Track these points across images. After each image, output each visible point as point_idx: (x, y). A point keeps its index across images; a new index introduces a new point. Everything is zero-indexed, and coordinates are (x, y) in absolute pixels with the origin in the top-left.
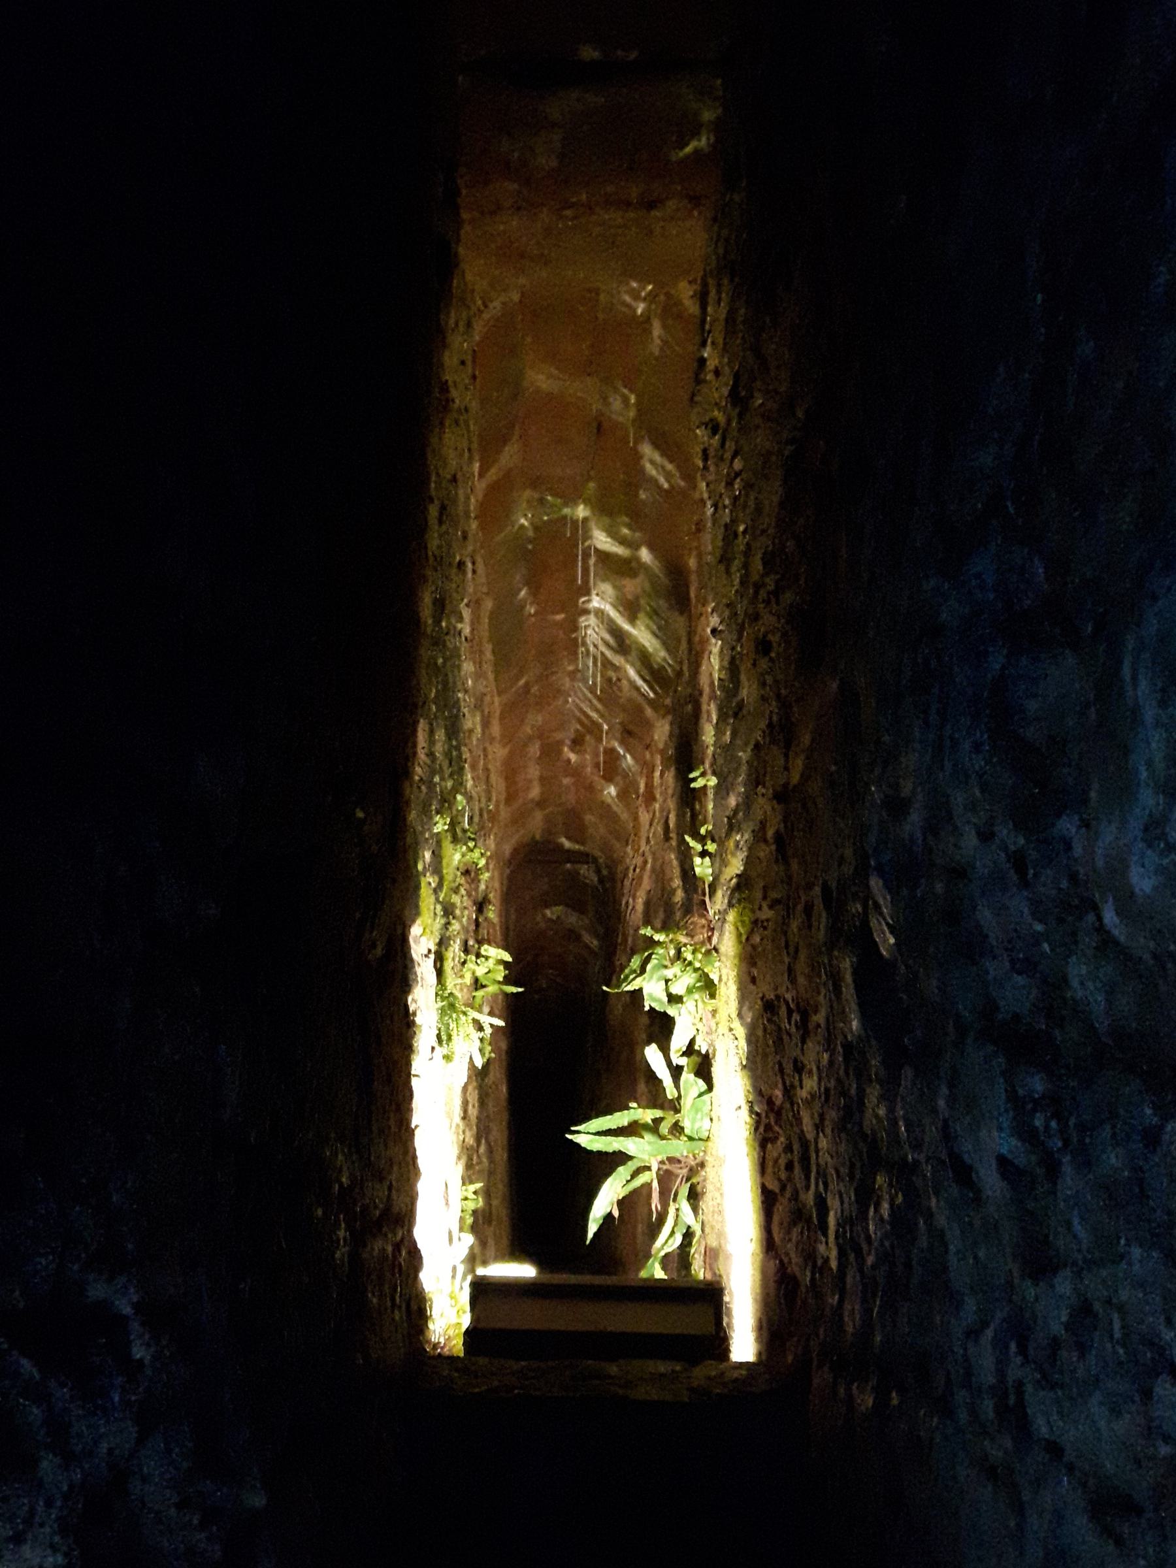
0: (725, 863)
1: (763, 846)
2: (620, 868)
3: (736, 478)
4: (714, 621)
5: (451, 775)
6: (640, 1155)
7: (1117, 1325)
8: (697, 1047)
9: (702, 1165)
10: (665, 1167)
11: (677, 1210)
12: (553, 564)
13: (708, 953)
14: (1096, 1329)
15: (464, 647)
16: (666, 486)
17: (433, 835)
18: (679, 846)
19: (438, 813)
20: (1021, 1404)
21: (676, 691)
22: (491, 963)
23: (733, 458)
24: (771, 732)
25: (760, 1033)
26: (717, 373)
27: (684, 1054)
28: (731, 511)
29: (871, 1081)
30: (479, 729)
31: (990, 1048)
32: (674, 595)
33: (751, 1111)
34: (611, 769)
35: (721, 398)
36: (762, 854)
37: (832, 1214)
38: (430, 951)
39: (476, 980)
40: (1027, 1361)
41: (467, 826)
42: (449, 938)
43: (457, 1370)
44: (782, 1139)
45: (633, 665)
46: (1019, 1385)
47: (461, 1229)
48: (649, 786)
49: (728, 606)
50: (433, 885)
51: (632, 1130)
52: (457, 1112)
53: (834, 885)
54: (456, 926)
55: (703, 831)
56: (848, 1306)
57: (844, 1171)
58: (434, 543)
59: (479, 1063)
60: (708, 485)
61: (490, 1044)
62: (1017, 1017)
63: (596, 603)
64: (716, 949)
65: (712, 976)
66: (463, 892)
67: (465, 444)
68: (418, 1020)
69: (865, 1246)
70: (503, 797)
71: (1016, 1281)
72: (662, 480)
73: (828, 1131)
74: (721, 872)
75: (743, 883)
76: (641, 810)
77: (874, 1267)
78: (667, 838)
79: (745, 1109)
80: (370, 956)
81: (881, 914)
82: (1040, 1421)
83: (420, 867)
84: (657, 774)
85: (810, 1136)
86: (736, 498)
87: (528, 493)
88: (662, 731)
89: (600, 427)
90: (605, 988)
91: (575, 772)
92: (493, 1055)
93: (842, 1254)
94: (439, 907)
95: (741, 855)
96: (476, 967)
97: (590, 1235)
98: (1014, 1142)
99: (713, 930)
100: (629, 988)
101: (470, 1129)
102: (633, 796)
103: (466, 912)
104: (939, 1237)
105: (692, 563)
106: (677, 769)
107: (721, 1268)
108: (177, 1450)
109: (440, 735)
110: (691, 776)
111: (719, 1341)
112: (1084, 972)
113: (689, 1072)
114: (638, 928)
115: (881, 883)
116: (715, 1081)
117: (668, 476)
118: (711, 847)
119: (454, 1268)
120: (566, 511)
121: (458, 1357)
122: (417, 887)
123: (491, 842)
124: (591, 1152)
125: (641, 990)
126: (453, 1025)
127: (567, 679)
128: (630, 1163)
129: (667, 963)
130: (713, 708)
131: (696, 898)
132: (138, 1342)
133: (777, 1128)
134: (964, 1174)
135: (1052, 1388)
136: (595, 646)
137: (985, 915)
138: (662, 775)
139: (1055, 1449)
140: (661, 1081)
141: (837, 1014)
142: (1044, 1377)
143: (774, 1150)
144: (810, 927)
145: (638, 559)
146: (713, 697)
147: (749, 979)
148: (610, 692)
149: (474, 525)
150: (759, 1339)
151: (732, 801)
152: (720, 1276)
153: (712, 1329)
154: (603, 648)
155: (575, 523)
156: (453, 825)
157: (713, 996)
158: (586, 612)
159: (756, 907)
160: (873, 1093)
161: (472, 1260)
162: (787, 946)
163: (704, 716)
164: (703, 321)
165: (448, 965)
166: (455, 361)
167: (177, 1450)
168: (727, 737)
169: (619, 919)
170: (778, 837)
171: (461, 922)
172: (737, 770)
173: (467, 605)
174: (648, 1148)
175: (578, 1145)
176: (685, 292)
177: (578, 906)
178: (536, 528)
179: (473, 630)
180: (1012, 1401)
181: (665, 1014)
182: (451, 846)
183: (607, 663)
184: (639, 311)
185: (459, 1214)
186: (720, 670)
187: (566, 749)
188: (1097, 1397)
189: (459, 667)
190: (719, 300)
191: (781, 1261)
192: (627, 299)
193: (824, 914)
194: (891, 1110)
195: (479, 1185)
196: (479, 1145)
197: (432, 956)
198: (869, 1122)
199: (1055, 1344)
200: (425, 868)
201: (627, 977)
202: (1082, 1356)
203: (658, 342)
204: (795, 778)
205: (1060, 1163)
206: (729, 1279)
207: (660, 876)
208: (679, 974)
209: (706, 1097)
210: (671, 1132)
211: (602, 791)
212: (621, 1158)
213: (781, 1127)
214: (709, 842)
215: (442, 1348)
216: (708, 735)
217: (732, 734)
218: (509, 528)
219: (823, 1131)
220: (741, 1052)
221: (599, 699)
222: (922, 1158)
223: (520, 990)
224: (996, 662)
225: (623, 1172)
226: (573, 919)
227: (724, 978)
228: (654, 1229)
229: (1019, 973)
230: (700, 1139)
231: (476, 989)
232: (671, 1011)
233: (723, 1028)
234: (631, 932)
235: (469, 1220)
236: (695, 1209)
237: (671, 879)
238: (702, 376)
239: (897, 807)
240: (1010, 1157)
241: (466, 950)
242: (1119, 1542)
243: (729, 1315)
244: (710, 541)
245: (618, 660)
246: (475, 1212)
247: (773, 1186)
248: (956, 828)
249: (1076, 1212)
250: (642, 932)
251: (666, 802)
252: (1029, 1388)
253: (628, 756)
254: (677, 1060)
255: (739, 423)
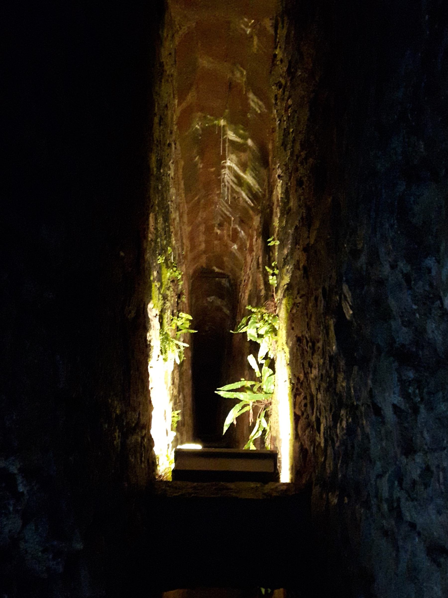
0: (282, 279)
1: (298, 271)
2: (239, 280)
3: (289, 108)
4: (279, 172)
5: (165, 239)
6: (245, 400)
7: (441, 478)
8: (269, 356)
9: (270, 403)
10: (256, 404)
11: (260, 421)
12: (210, 146)
13: (274, 317)
14: (432, 477)
15: (171, 182)
16: (259, 112)
17: (157, 264)
18: (263, 271)
19: (159, 255)
20: (399, 506)
21: (262, 203)
22: (183, 320)
23: (288, 99)
24: (302, 221)
25: (295, 350)
26: (282, 61)
27: (264, 359)
28: (287, 123)
29: (340, 371)
30: (178, 218)
31: (392, 359)
32: (262, 161)
33: (291, 382)
34: (235, 237)
35: (283, 72)
36: (297, 275)
37: (322, 425)
38: (157, 315)
39: (178, 327)
40: (402, 489)
41: (172, 261)
42: (165, 309)
43: (169, 486)
44: (303, 394)
45: (244, 191)
46: (399, 500)
47: (172, 430)
48: (251, 245)
49: (285, 165)
50: (158, 286)
51: (242, 389)
52: (170, 382)
53: (328, 289)
54: (168, 304)
55: (273, 264)
56: (327, 462)
57: (328, 408)
58: (156, 135)
59: (178, 362)
60: (277, 111)
61: (184, 354)
62: (403, 346)
63: (228, 163)
64: (277, 315)
65: (276, 327)
66: (171, 289)
67: (171, 91)
68: (152, 344)
69: (335, 439)
70: (189, 249)
71: (399, 456)
72: (257, 109)
73: (322, 391)
74: (280, 282)
75: (290, 287)
76: (247, 255)
77: (338, 447)
78: (258, 268)
79: (288, 381)
80: (129, 317)
81: (347, 301)
82: (407, 514)
83: (152, 278)
84: (254, 240)
85: (314, 392)
86: (289, 117)
87: (199, 114)
88: (256, 221)
89: (231, 86)
90: (231, 331)
91: (220, 238)
92: (185, 358)
93: (326, 440)
94: (161, 296)
95: (289, 275)
96: (177, 322)
97: (225, 431)
98: (400, 398)
99: (276, 307)
100: (241, 331)
101: (176, 388)
102: (243, 250)
103: (173, 298)
104: (367, 437)
105: (270, 147)
106: (262, 237)
107: (277, 444)
108: (41, 529)
109: (160, 220)
110: (269, 240)
111: (276, 475)
112: (434, 326)
113: (266, 366)
114: (246, 306)
115: (347, 288)
116: (276, 370)
117: (260, 107)
118: (276, 272)
119: (168, 445)
120: (216, 122)
121: (169, 481)
122: (150, 287)
123: (184, 268)
124: (225, 398)
125: (246, 332)
126: (167, 346)
127: (216, 197)
128: (241, 403)
129: (257, 321)
130: (278, 210)
131: (270, 293)
132: (21, 485)
133: (301, 390)
134: (378, 411)
135: (412, 500)
136: (228, 182)
137: (392, 303)
138: (256, 240)
139: (413, 526)
140: (254, 370)
141: (327, 343)
142: (409, 496)
143: (299, 399)
144: (317, 306)
145: (247, 144)
146: (278, 205)
147: (291, 328)
148: (235, 203)
149: (176, 127)
150: (292, 473)
151: (286, 252)
152: (277, 447)
153: (273, 471)
154: (231, 183)
155: (220, 127)
156: (166, 260)
157: (276, 335)
158: (224, 167)
159: (295, 297)
160: (341, 377)
161: (177, 441)
162: (307, 314)
163: (274, 214)
164: (276, 37)
165: (165, 321)
166: (167, 53)
167: (41, 529)
168: (284, 223)
169: (238, 302)
170: (304, 267)
171: (171, 303)
172: (288, 237)
173: (173, 163)
174: (248, 397)
175: (219, 396)
176: (268, 23)
177: (221, 297)
178: (203, 129)
179: (175, 175)
180: (395, 505)
181: (256, 342)
182: (166, 269)
183: (233, 191)
184: (248, 32)
185: (171, 423)
186: (281, 194)
187: (216, 228)
188: (431, 507)
189: (169, 191)
190: (283, 27)
191: (301, 443)
192: (243, 26)
193: (323, 302)
194: (348, 384)
195: (179, 411)
196: (179, 395)
197: (158, 317)
198: (339, 388)
199: (414, 483)
200: (154, 279)
201: (240, 327)
202: (426, 488)
203: (256, 47)
204: (312, 242)
205: (419, 407)
206: (280, 449)
207: (255, 284)
208: (262, 325)
209: (273, 376)
210: (258, 390)
211: (231, 247)
212: (236, 401)
213: (302, 389)
214: (276, 269)
215: (163, 477)
216: (276, 223)
217: (286, 222)
218: (191, 129)
219: (320, 391)
220: (287, 358)
221: (230, 206)
222: (360, 403)
223: (196, 331)
224: (402, 187)
225: (238, 407)
226: (219, 302)
227: (281, 328)
228: (251, 429)
229: (405, 326)
230: (270, 393)
231: (178, 331)
232: (259, 341)
233: (280, 348)
234: (243, 307)
235: (175, 425)
236: (267, 421)
237: (260, 285)
238: (275, 62)
239: (355, 253)
240: (398, 405)
241: (173, 315)
242: (439, 565)
243: (280, 463)
244: (278, 136)
245: (238, 189)
246: (178, 422)
247: (299, 413)
248: (381, 263)
249: (425, 429)
250: (247, 308)
251: (258, 251)
252: (403, 500)
253: (242, 232)
254: (261, 361)
255: (290, 83)
